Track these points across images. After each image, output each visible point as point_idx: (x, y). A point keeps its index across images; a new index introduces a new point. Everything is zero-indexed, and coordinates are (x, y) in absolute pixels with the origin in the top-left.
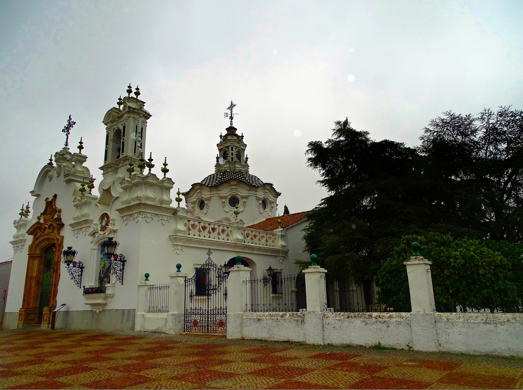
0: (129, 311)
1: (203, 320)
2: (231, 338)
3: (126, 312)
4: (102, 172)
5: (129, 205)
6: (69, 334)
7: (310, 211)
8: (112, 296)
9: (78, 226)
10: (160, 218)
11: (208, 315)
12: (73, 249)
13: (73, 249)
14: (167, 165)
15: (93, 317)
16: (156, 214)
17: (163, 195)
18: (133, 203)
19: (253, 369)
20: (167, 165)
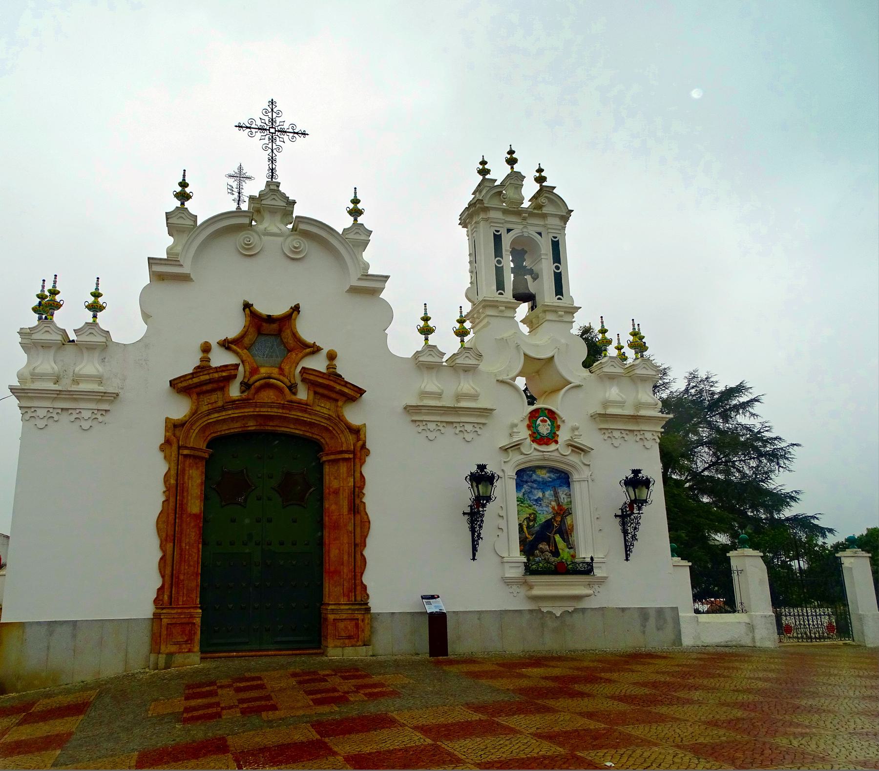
0: (660, 611)
1: (800, 624)
2: (872, 646)
3: (653, 614)
4: (576, 305)
5: (74, 388)
6: (545, 658)
7: (175, 490)
8: (602, 581)
9: (441, 415)
10: (639, 437)
11: (808, 616)
12: (488, 470)
13: (488, 470)
14: (606, 331)
15: (543, 625)
16: (630, 431)
17: (637, 392)
18: (84, 387)
19: (647, 729)
20: (606, 331)
